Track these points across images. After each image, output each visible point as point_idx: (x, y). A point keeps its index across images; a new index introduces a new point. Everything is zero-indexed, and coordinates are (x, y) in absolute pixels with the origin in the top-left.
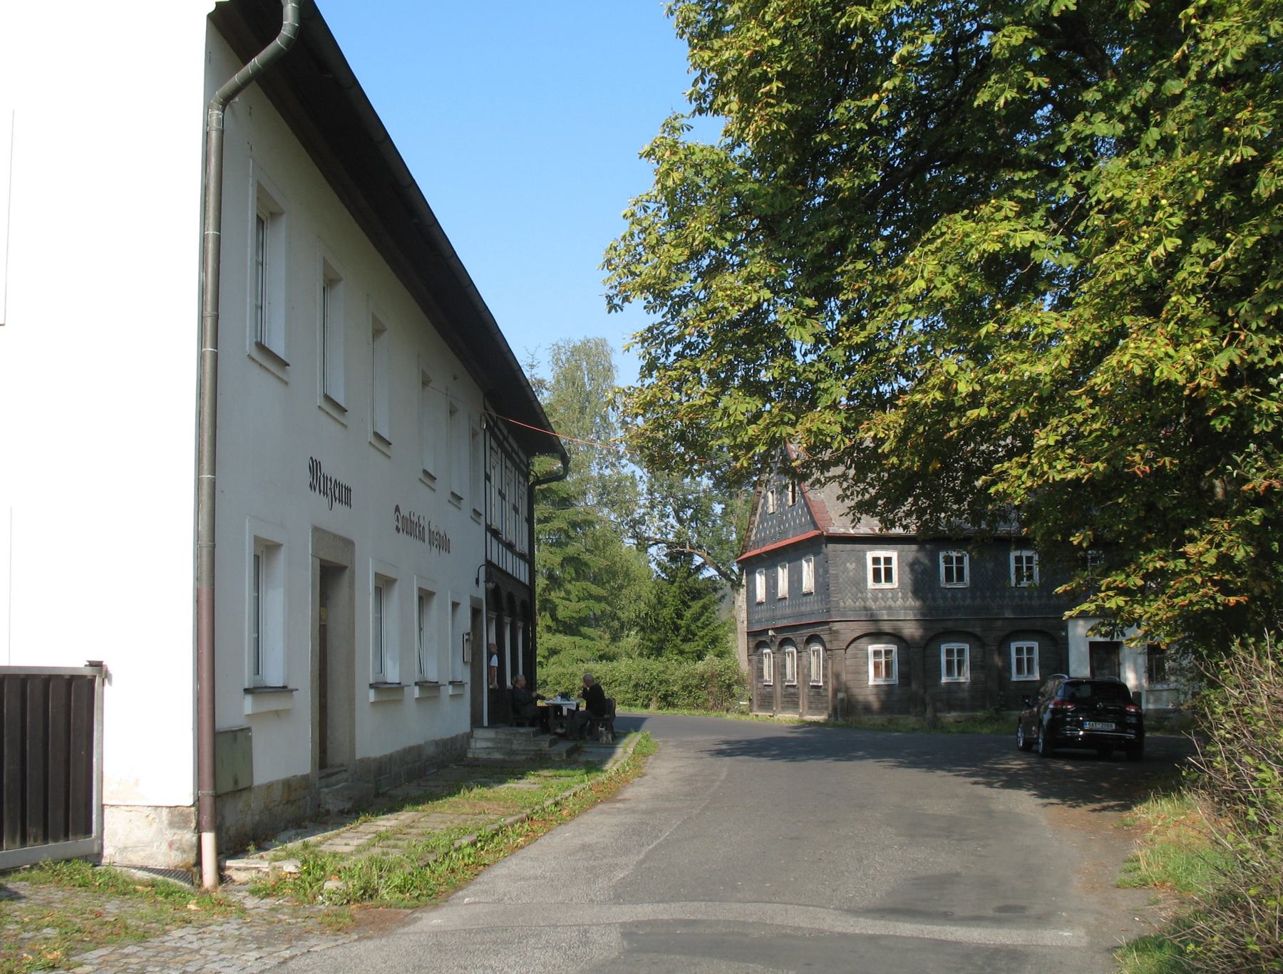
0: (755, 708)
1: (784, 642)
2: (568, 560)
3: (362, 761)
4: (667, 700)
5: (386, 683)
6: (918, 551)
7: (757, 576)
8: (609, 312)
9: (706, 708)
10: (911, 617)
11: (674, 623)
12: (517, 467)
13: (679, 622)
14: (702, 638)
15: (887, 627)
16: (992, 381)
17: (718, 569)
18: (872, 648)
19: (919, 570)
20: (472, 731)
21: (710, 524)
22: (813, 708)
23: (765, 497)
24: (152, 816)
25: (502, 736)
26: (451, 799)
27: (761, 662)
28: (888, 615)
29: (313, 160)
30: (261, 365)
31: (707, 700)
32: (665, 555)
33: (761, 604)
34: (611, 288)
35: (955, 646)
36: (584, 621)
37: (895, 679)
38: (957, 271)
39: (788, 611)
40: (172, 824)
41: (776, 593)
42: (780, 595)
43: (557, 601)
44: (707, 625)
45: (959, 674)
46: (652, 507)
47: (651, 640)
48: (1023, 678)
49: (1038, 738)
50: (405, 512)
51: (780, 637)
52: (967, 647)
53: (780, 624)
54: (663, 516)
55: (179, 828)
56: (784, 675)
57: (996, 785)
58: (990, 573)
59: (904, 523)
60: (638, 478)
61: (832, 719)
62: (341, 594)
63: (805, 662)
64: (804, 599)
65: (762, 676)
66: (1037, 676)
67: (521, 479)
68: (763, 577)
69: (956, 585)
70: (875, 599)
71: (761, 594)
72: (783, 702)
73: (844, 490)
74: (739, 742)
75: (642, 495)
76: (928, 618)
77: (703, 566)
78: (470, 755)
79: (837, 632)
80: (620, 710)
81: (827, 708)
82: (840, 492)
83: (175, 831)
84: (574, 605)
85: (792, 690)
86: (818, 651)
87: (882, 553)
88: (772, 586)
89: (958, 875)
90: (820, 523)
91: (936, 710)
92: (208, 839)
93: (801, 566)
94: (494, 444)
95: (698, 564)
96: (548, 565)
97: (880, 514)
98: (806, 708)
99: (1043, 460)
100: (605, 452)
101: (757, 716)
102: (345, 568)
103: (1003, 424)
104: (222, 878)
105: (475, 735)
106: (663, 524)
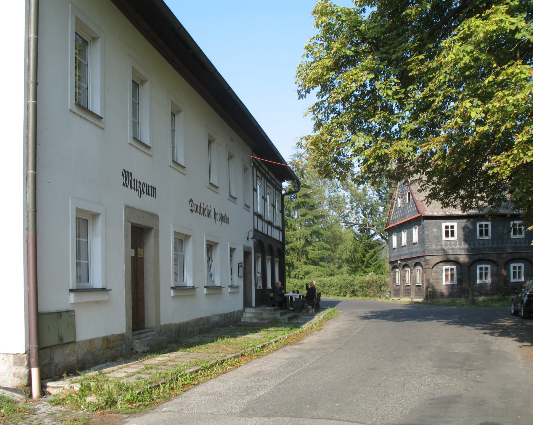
0: (392, 296)
1: (405, 266)
2: (314, 233)
3: (166, 325)
4: (354, 293)
5: (186, 287)
6: (467, 222)
7: (393, 236)
8: (299, 99)
9: (370, 296)
10: (463, 253)
11: (362, 260)
13: (364, 259)
14: (374, 266)
15: (452, 258)
16: (490, 108)
17: (381, 235)
18: (444, 268)
19: (467, 231)
20: (244, 309)
21: (378, 216)
22: (417, 296)
23: (397, 200)
24: (5, 359)
25: (259, 311)
26: (212, 344)
27: (395, 275)
28: (452, 252)
29: (123, 13)
30: (81, 116)
31: (370, 293)
32: (358, 230)
33: (394, 249)
34: (299, 86)
35: (484, 266)
36: (322, 259)
37: (455, 282)
38: (472, 48)
39: (406, 252)
40: (15, 364)
41: (401, 244)
42: (403, 245)
43: (309, 251)
44: (376, 260)
45: (486, 279)
46: (352, 209)
47: (352, 267)
48: (516, 280)
49: (521, 309)
51: (403, 264)
53: (403, 257)
54: (357, 213)
55: (19, 366)
56: (405, 281)
57: (496, 334)
59: (454, 204)
60: (346, 196)
61: (425, 300)
62: (150, 241)
63: (414, 275)
64: (413, 246)
65: (395, 282)
66: (523, 279)
67: (277, 193)
68: (396, 237)
70: (446, 245)
71: (395, 245)
72: (404, 293)
73: (421, 187)
74: (377, 312)
75: (348, 204)
76: (471, 253)
77: (375, 234)
78: (242, 320)
79: (428, 260)
80: (323, 297)
81: (423, 296)
82: (419, 188)
83: (17, 367)
84: (316, 252)
85: (408, 288)
86: (420, 270)
87: (449, 223)
88: (399, 240)
89: (460, 396)
90: (421, 211)
91: (474, 296)
92: (35, 372)
93: (412, 231)
95: (372, 233)
96: (305, 235)
97: (442, 200)
98: (414, 295)
99: (520, 151)
100: (331, 186)
101: (393, 299)
102: (151, 228)
103: (498, 135)
104: (43, 392)
105: (246, 311)
106: (357, 216)
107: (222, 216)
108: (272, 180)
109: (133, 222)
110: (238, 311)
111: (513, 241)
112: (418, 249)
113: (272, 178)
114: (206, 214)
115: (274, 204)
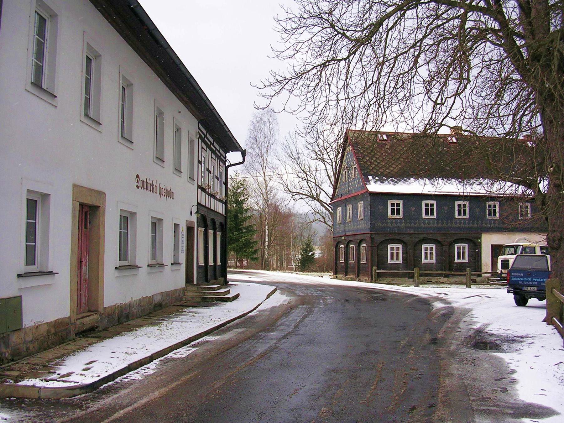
12: (219, 158)
48: (460, 261)
50: (142, 178)
52: (434, 246)
53: (347, 234)
58: (446, 212)
67: (221, 164)
69: (396, 216)
94: (204, 146)
107: (167, 190)
108: (217, 152)
109: (80, 201)
110: (180, 289)
111: (458, 222)
112: (364, 226)
113: (216, 149)
114: (151, 190)
115: (210, 170)
